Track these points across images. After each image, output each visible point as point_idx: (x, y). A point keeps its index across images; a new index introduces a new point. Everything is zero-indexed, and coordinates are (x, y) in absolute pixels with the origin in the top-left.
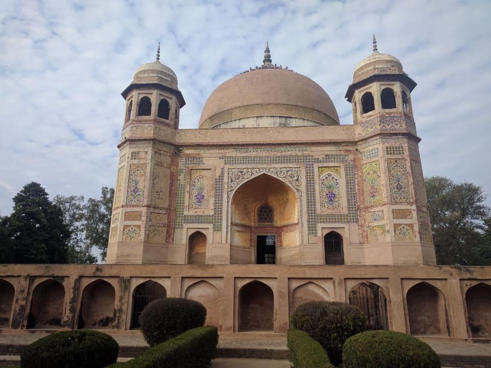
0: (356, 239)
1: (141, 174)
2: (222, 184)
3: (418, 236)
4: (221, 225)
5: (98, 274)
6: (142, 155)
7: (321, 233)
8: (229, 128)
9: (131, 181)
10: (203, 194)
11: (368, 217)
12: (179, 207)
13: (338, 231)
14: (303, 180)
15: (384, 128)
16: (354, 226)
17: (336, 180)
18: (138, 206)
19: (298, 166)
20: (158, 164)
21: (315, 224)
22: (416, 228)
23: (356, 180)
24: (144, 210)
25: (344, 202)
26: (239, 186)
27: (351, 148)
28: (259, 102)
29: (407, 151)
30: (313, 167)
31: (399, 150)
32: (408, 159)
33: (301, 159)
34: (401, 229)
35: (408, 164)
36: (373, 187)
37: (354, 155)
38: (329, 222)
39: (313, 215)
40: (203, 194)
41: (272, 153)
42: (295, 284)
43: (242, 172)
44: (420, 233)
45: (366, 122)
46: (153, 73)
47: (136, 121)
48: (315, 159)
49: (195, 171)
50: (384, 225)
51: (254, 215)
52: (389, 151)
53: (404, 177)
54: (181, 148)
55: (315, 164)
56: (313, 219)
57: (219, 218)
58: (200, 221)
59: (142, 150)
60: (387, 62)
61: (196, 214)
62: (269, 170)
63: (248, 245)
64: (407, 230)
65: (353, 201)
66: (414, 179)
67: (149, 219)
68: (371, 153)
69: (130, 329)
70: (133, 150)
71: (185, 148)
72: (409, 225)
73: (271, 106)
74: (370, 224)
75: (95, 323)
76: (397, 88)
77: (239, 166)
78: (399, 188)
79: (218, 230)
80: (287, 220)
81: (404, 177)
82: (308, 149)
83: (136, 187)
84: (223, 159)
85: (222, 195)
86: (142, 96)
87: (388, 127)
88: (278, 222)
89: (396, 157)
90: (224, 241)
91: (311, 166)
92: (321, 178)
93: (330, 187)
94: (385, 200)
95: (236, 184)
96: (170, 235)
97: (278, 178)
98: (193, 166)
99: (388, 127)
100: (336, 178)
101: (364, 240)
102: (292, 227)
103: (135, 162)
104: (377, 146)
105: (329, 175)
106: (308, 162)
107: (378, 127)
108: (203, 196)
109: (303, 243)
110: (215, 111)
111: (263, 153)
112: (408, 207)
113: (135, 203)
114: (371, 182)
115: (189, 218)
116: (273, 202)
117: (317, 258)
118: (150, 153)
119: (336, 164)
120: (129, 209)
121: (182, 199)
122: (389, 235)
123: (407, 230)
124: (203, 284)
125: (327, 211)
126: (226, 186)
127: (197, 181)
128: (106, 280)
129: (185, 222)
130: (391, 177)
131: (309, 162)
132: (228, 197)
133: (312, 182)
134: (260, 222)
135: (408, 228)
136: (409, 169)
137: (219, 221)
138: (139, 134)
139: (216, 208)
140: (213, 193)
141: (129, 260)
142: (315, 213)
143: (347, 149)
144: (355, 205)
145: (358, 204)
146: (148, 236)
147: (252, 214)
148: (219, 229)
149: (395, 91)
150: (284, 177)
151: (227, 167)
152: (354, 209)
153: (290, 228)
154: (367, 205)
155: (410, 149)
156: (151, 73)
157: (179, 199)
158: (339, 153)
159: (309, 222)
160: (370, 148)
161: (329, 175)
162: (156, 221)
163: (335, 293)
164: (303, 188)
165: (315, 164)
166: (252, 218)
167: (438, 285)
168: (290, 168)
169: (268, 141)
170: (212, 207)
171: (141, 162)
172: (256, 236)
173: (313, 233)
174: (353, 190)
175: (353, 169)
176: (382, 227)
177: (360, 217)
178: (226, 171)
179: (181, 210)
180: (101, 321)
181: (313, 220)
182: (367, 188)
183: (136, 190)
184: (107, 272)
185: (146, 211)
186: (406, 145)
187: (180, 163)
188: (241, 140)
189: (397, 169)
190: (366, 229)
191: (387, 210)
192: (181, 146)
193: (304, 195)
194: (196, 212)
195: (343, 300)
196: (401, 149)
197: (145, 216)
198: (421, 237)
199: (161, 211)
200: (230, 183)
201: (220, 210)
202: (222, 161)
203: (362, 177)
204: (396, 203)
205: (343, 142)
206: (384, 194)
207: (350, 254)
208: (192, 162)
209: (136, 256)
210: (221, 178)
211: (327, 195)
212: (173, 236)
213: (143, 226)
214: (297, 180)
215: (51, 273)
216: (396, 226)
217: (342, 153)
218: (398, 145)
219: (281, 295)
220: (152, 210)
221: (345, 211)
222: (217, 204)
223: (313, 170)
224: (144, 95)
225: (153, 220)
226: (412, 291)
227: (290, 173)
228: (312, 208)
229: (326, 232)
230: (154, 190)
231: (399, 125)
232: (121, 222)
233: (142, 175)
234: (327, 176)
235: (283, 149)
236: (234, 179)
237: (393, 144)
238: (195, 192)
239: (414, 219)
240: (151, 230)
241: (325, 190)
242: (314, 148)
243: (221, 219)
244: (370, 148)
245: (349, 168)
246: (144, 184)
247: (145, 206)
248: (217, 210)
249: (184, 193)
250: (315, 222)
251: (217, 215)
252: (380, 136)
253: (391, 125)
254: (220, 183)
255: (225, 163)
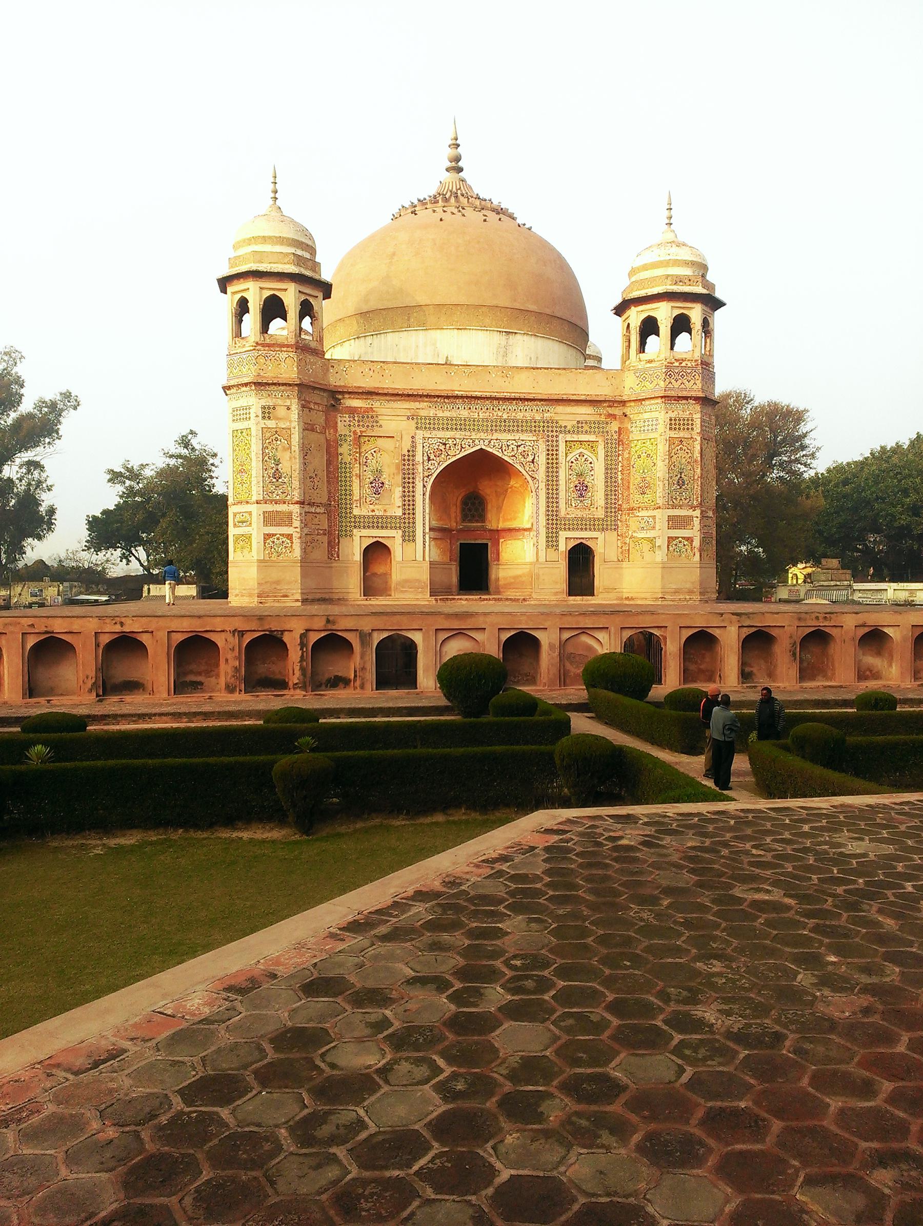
0: (612, 554)
1: (284, 447)
2: (413, 465)
3: (698, 555)
4: (413, 532)
5: (330, 627)
6: (281, 411)
7: (563, 547)
8: (423, 364)
9: (266, 458)
10: (382, 480)
11: (633, 523)
12: (344, 501)
13: (588, 543)
14: (542, 460)
15: (670, 386)
16: (612, 536)
17: (591, 463)
18: (285, 503)
19: (535, 438)
20: (308, 428)
21: (557, 533)
22: (697, 543)
23: (620, 464)
24: (296, 509)
25: (599, 496)
26: (438, 471)
27: (617, 411)
28: (463, 300)
29: (699, 426)
30: (557, 441)
31: (686, 424)
32: (699, 438)
33: (539, 427)
34: (676, 545)
35: (698, 448)
36: (644, 479)
37: (621, 423)
38: (577, 529)
39: (554, 518)
40: (382, 480)
41: (495, 414)
42: (566, 635)
43: (445, 444)
44: (701, 550)
45: (645, 370)
46: (289, 245)
47: (263, 345)
48: (561, 427)
49: (366, 439)
50: (655, 538)
51: (455, 511)
52: (674, 424)
53: (690, 467)
54: (340, 397)
55: (561, 436)
56: (555, 523)
57: (411, 521)
58: (380, 525)
59: (279, 402)
60: (687, 263)
61: (373, 514)
62: (490, 442)
63: (447, 559)
64: (684, 545)
65: (613, 497)
66: (702, 470)
67: (304, 524)
68: (646, 424)
69: (377, 690)
70: (263, 402)
71: (347, 396)
72: (688, 539)
73: (484, 309)
74: (635, 535)
75: (321, 684)
76: (696, 313)
77: (441, 434)
78: (681, 483)
79: (409, 541)
80: (511, 520)
81: (690, 467)
82: (551, 409)
83: (277, 470)
84: (413, 419)
85: (413, 483)
86: (267, 294)
87: (676, 385)
88: (494, 521)
89: (682, 434)
90: (419, 557)
91: (555, 439)
92: (568, 459)
93: (580, 475)
94: (660, 502)
95: (436, 465)
96: (333, 546)
97: (503, 457)
98: (363, 429)
99: (676, 385)
100: (590, 460)
101: (625, 555)
102: (518, 533)
103: (271, 424)
104: (654, 415)
105: (581, 455)
106: (550, 431)
107: (662, 384)
108: (383, 483)
109: (537, 560)
110: (373, 305)
111: (479, 413)
112: (690, 512)
113: (278, 497)
114: (641, 471)
115: (362, 520)
116: (486, 488)
117: (557, 583)
118: (295, 408)
119: (592, 438)
120: (269, 508)
121: (348, 488)
122: (660, 553)
123: (684, 545)
124: (460, 636)
125: (574, 513)
126: (420, 468)
127: (370, 457)
128: (339, 633)
129: (355, 527)
130: (672, 466)
131: (552, 431)
132: (424, 486)
133: (555, 465)
134: (464, 521)
135: (686, 543)
136: (697, 455)
137: (411, 525)
138: (271, 373)
139: (404, 505)
140: (399, 479)
141: (280, 590)
142: (557, 515)
143: (610, 412)
144: (615, 503)
145: (620, 502)
146: (304, 551)
147: (453, 509)
148: (411, 538)
149: (693, 321)
150: (513, 456)
151: (420, 434)
152: (613, 510)
153: (513, 533)
154: (632, 505)
155: (702, 421)
156: (276, 244)
157: (343, 488)
158: (597, 418)
159: (548, 528)
160: (646, 416)
161: (581, 455)
162: (313, 527)
163: (610, 644)
164: (541, 474)
165: (561, 436)
166: (453, 515)
167: (716, 633)
168: (523, 440)
169: (487, 391)
170: (399, 503)
171: (282, 425)
172: (458, 543)
173: (553, 546)
174: (613, 480)
175: (620, 441)
176: (652, 540)
177: (621, 521)
178: (419, 441)
179: (348, 506)
180: (329, 680)
181: (554, 526)
182: (635, 479)
183: (277, 475)
184: (343, 624)
185: (298, 511)
186: (699, 416)
187: (339, 424)
188: (443, 387)
189: (681, 453)
190: (627, 540)
191: (662, 516)
192: (343, 393)
193: (542, 486)
194: (373, 511)
195: (618, 651)
196: (690, 422)
197: (299, 519)
198: (701, 556)
199: (318, 510)
200: (426, 463)
201: (411, 507)
202: (412, 423)
203: (629, 459)
204: (674, 507)
205: (605, 401)
206: (659, 493)
207: (601, 574)
208: (361, 423)
209: (289, 583)
210: (411, 453)
211: (576, 486)
212: (338, 549)
213: (296, 536)
214: (533, 462)
215: (267, 627)
216: (670, 539)
217: (603, 418)
218: (686, 415)
219: (551, 646)
220: (307, 508)
221: (600, 514)
222: (406, 499)
223: (557, 446)
224: (272, 292)
225: (310, 525)
226: (690, 640)
227: (521, 449)
228: (553, 507)
229: (572, 544)
230: (308, 477)
231: (693, 381)
232: (259, 529)
233: (284, 449)
234: (577, 456)
235: (513, 406)
236: (432, 457)
237: (681, 413)
238: (369, 477)
239: (694, 532)
240: (308, 544)
241: (574, 478)
242: (560, 409)
243: (414, 523)
244: (646, 416)
245: (612, 444)
246: (291, 464)
247: (297, 503)
248: (407, 507)
249: (350, 477)
250: (556, 528)
251: (406, 516)
252: (663, 400)
253: (680, 382)
254: (411, 463)
255: (417, 428)
